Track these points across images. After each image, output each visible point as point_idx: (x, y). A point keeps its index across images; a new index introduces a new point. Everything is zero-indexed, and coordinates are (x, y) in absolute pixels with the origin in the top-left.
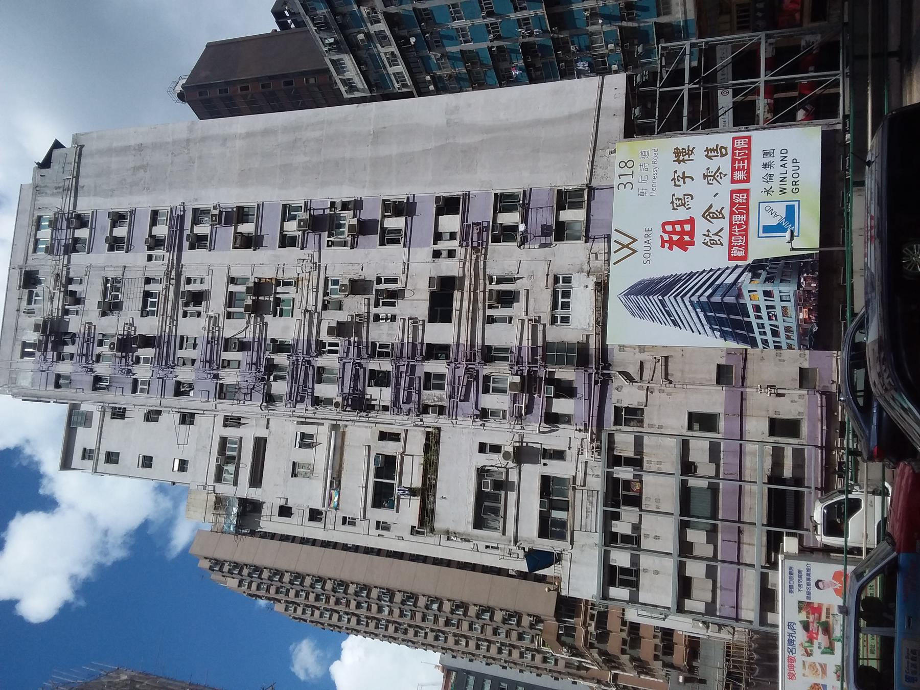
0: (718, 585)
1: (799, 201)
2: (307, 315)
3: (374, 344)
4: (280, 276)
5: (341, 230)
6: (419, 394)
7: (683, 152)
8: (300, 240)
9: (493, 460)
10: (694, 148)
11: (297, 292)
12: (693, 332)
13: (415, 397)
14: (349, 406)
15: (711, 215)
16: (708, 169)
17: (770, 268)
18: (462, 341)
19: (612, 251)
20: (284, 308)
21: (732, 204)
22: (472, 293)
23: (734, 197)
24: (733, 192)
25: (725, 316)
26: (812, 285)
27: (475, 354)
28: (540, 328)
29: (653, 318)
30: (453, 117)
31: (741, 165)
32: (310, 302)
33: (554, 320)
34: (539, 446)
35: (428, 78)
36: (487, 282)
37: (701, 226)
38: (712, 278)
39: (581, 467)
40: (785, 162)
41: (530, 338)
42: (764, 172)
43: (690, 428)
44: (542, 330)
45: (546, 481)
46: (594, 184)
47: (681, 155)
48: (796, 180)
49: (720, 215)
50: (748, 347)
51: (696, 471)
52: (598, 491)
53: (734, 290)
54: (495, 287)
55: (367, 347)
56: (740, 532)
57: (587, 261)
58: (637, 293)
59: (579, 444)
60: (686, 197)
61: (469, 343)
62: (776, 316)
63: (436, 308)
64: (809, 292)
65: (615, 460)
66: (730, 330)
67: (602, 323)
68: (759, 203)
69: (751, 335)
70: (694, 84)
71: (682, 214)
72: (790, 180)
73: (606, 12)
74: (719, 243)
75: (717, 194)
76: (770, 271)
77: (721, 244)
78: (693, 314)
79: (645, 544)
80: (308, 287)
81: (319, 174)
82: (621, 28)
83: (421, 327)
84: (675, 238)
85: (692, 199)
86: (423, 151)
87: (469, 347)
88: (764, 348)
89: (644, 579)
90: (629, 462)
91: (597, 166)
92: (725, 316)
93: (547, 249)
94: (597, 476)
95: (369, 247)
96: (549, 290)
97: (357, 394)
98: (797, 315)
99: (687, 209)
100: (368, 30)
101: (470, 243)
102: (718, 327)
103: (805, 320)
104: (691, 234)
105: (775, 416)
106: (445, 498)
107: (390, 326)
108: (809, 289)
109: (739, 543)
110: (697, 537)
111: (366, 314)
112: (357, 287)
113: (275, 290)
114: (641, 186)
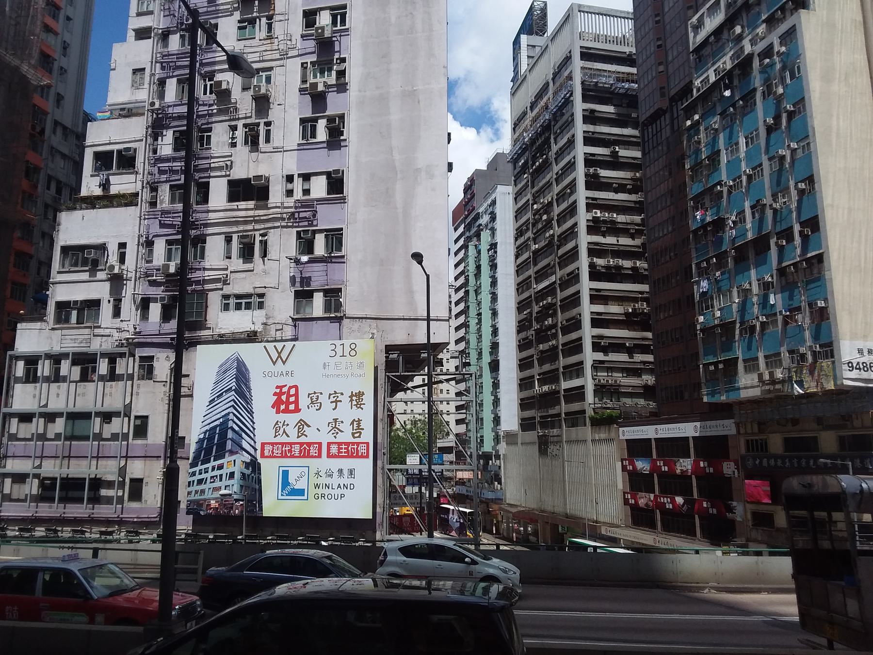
0: (28, 443)
1: (307, 500)
3: (210, 130)
4: (276, 18)
5: (318, 74)
6: (166, 182)
7: (359, 399)
8: (309, 32)
9: (113, 258)
10: (362, 409)
11: (260, 40)
12: (204, 416)
13: (164, 177)
14: (157, 116)
15: (301, 427)
16: (342, 422)
18: (212, 215)
20: (247, 29)
22: (252, 219)
24: (320, 444)
25: (216, 442)
26: (237, 511)
27: (198, 228)
28: (219, 285)
29: (217, 383)
30: (423, 174)
31: (343, 450)
33: (226, 297)
35: (696, 117)
36: (261, 232)
37: (292, 419)
39: (107, 332)
40: (342, 488)
41: (211, 277)
42: (335, 470)
43: (137, 417)
44: (218, 287)
45: (94, 304)
46: (345, 322)
47: (357, 398)
48: (326, 497)
49: (301, 433)
50: (190, 461)
51: (107, 423)
52: (89, 347)
54: (258, 239)
55: (208, 123)
56: (56, 457)
57: (276, 322)
59: (125, 329)
60: (319, 404)
61: (209, 221)
62: (213, 482)
63: (241, 185)
64: (232, 508)
65: (112, 358)
66: (204, 446)
67: (222, 339)
68: (309, 467)
69: (200, 463)
71: (304, 401)
72: (326, 491)
73: (748, 305)
74: (277, 434)
76: (251, 476)
79: (54, 386)
80: (264, 51)
81: (376, 38)
82: (734, 322)
83: (224, 173)
85: (317, 410)
86: (392, 148)
87: (201, 222)
88: (189, 473)
89: (30, 387)
90: (112, 370)
91: (361, 322)
92: (216, 442)
93: (288, 284)
94: (101, 346)
95: (300, 108)
96: (252, 290)
97: (166, 121)
98: (213, 499)
99: (308, 406)
100: (746, 37)
101: (298, 210)
102: (207, 437)
104: (287, 411)
105: (144, 482)
106: (83, 219)
107: (226, 143)
108: (234, 509)
109: (13, 456)
110: (59, 426)
111: (237, 117)
112: (262, 103)
113: (263, 16)
114: (332, 365)
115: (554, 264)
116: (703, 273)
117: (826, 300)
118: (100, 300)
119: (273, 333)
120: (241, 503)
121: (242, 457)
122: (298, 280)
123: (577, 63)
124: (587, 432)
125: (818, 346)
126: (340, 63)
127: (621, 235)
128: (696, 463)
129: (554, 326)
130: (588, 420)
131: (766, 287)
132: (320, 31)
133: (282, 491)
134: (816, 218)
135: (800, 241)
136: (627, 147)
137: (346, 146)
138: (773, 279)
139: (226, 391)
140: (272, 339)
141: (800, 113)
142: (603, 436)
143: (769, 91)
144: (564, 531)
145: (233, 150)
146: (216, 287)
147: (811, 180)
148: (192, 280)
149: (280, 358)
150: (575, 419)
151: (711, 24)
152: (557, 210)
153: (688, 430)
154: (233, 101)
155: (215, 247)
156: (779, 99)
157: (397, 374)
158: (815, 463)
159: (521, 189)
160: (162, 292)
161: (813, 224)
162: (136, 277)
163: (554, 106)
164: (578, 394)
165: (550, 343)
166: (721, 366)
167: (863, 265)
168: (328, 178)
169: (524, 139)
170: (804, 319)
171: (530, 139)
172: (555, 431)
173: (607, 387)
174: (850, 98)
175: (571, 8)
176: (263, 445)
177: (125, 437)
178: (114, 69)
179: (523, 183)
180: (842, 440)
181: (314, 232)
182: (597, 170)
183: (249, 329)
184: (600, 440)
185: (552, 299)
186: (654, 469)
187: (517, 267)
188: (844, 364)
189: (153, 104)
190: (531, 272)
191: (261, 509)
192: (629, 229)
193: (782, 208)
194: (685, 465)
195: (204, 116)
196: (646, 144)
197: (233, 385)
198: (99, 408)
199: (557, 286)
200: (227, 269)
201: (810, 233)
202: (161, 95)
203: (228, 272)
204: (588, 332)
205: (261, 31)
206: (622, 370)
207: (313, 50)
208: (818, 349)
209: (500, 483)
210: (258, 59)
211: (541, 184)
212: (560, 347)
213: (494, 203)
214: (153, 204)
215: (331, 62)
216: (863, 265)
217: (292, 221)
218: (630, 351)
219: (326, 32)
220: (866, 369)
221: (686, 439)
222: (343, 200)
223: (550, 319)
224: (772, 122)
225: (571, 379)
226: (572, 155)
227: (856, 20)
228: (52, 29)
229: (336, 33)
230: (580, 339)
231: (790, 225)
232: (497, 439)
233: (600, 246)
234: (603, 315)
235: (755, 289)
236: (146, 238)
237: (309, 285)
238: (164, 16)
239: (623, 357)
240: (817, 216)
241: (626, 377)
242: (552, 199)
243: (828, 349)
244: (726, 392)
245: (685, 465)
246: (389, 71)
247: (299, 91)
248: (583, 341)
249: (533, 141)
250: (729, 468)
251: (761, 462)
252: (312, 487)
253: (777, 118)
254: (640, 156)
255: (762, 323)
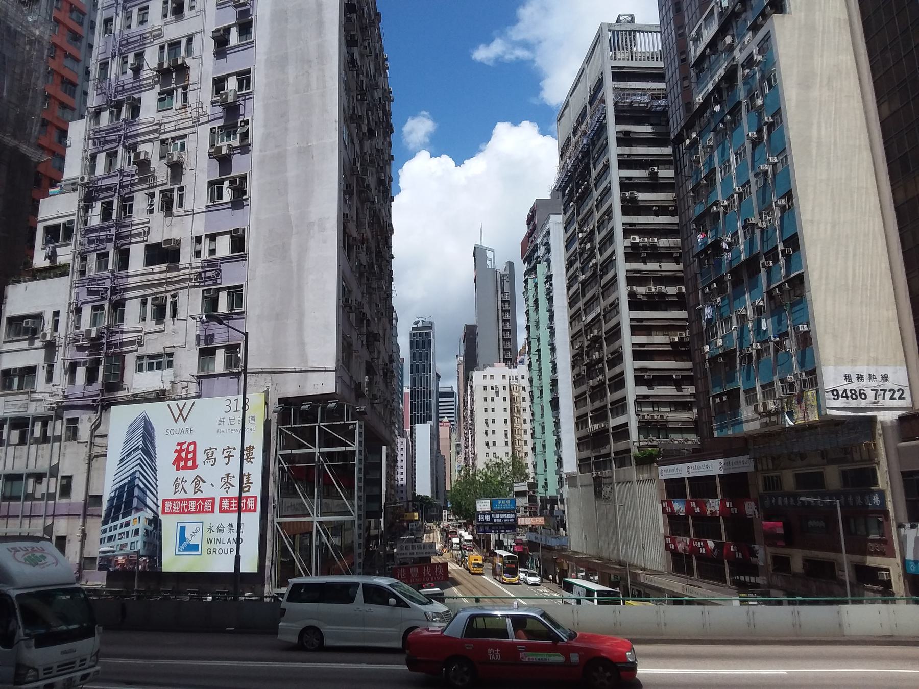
2: (157, 127)
3: (132, 199)
4: (190, 88)
5: (225, 138)
7: (249, 453)
9: (48, 327)
10: (252, 463)
11: (176, 110)
13: (92, 247)
16: (234, 477)
17: (154, 533)
18: (131, 280)
19: (177, 402)
21: (204, 500)
22: (165, 281)
23: (209, 501)
24: (213, 499)
25: (124, 500)
28: (134, 347)
29: (126, 442)
30: (316, 227)
32: (168, 125)
33: (140, 358)
34: (55, 361)
37: (189, 475)
38: (151, 488)
39: (41, 396)
41: (128, 340)
43: (63, 477)
44: (134, 349)
45: (31, 371)
48: (217, 552)
49: (197, 489)
53: (142, 506)
54: (169, 300)
58: (145, 428)
60: (214, 460)
61: (128, 286)
62: (121, 539)
65: (45, 421)
67: (136, 399)
69: (110, 520)
70: (318, 458)
71: (201, 457)
72: (218, 546)
73: (745, 331)
74: (177, 490)
75: (213, 486)
77: (175, 493)
78: (127, 474)
80: (179, 120)
83: (142, 239)
84: (183, 454)
85: (212, 465)
86: (288, 204)
87: (122, 287)
92: (124, 500)
93: (194, 342)
94: (36, 410)
95: (209, 171)
96: (163, 350)
103: (117, 561)
104: (186, 467)
111: (155, 184)
112: (176, 169)
113: (179, 87)
114: (227, 421)
115: (599, 294)
116: (708, 299)
117: (808, 324)
118: (36, 366)
119: (179, 390)
120: (144, 559)
121: (146, 514)
122: (202, 338)
123: (609, 84)
124: (632, 471)
125: (803, 373)
126: (244, 126)
127: (663, 260)
128: (722, 503)
129: (601, 360)
130: (632, 459)
131: (759, 311)
132: (224, 97)
133: (179, 547)
134: (796, 235)
135: (784, 261)
136: (667, 167)
137: (248, 205)
138: (764, 303)
139: (134, 450)
140: (178, 397)
141: (778, 124)
142: (646, 476)
143: (751, 105)
144: (616, 580)
145: (150, 217)
146: (132, 349)
147: (789, 195)
148: (113, 343)
149: (182, 416)
150: (622, 458)
151: (708, 35)
152: (598, 238)
153: (713, 467)
154: (152, 170)
155: (132, 309)
156: (760, 111)
157: (288, 426)
158: (796, 501)
159: (569, 217)
160: (88, 356)
161: (794, 242)
162: (65, 343)
163: (590, 130)
164: (622, 432)
165: (598, 379)
166: (725, 398)
167: (850, 283)
168: (232, 237)
169: (568, 166)
170: (791, 345)
171: (573, 165)
172: (607, 472)
173: (653, 423)
174: (834, 103)
175: (601, 29)
176: (164, 501)
177: (51, 496)
178: (70, 147)
179: (571, 211)
180: (844, 474)
181: (218, 290)
182: (634, 194)
183: (158, 389)
184: (644, 481)
185: (598, 332)
186: (689, 510)
187: (570, 299)
188: (827, 392)
189: (83, 179)
190: (580, 304)
191: (161, 565)
192: (672, 253)
193: (767, 227)
194: (714, 505)
195: (127, 186)
196: (678, 163)
197: (141, 443)
198: (31, 468)
199: (602, 317)
200: (141, 331)
201: (792, 252)
202: (93, 168)
203: (142, 334)
204: (629, 366)
205: (177, 103)
206: (670, 404)
207: (221, 115)
208: (804, 377)
209: (565, 529)
210: (174, 128)
211: (585, 212)
212: (607, 382)
213: (548, 233)
214: (83, 273)
215: (236, 126)
216: (850, 283)
217: (198, 280)
218: (678, 384)
219: (229, 97)
220: (854, 397)
221: (713, 477)
222: (244, 257)
223: (597, 353)
224: (756, 136)
225: (618, 417)
226: (607, 181)
227: (840, 19)
228: (67, 105)
229: (239, 97)
230: (622, 373)
231: (775, 245)
232: (560, 482)
233: (641, 273)
234: (646, 346)
235: (750, 315)
236: (76, 305)
237: (212, 341)
238: (97, 95)
239: (670, 390)
240: (796, 234)
241: (675, 411)
242: (594, 226)
243: (812, 377)
244: (732, 425)
245: (714, 505)
246: (286, 129)
247: (209, 155)
248: (625, 375)
249: (575, 167)
250: (750, 508)
251: (776, 501)
252: (205, 542)
253: (759, 131)
254: (673, 175)
255: (758, 351)
